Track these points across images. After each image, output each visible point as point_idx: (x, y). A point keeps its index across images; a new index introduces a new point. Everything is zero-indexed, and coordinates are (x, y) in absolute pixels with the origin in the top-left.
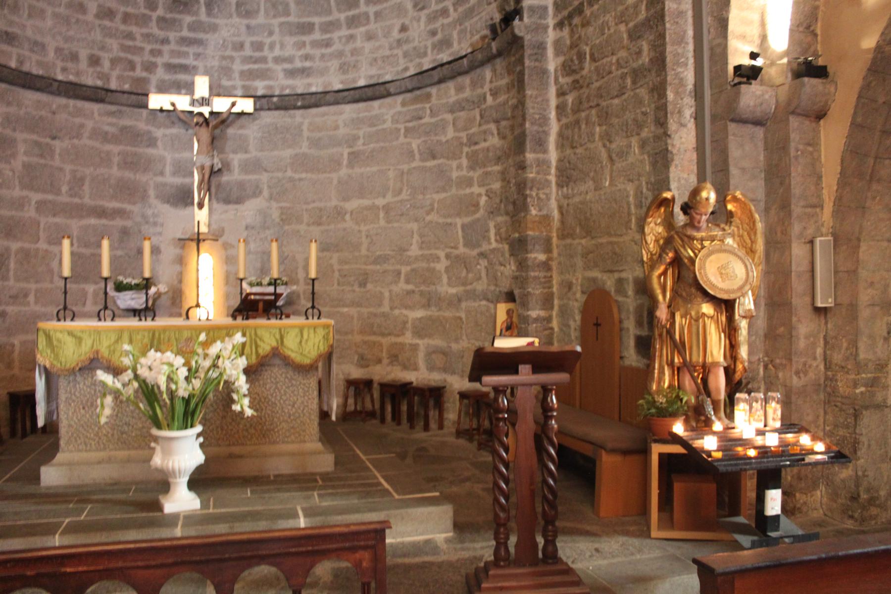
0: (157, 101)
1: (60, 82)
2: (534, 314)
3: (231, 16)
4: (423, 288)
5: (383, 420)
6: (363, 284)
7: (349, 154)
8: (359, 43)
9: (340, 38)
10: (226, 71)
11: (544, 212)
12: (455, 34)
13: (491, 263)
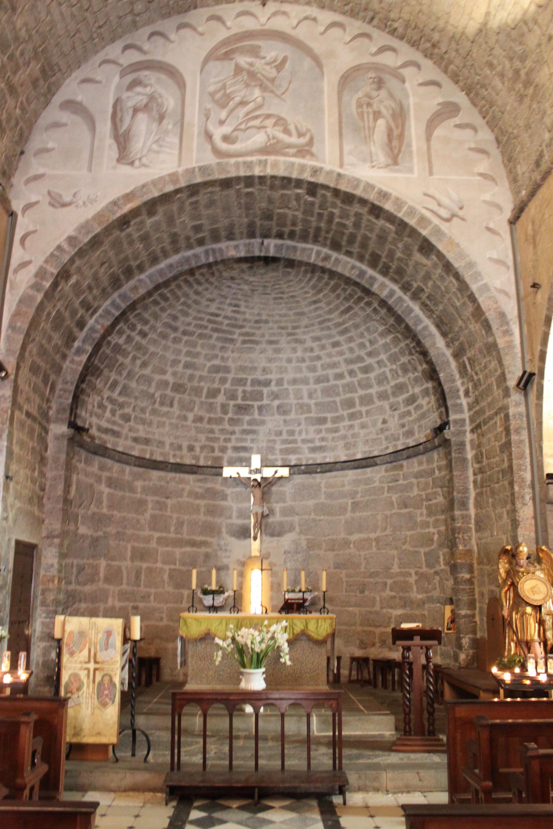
0: (228, 472)
1: (172, 464)
2: (463, 612)
3: (274, 414)
4: (401, 594)
5: (375, 686)
6: (362, 592)
7: (352, 503)
8: (356, 430)
9: (344, 427)
10: (271, 450)
11: (468, 548)
12: (416, 427)
13: (441, 578)
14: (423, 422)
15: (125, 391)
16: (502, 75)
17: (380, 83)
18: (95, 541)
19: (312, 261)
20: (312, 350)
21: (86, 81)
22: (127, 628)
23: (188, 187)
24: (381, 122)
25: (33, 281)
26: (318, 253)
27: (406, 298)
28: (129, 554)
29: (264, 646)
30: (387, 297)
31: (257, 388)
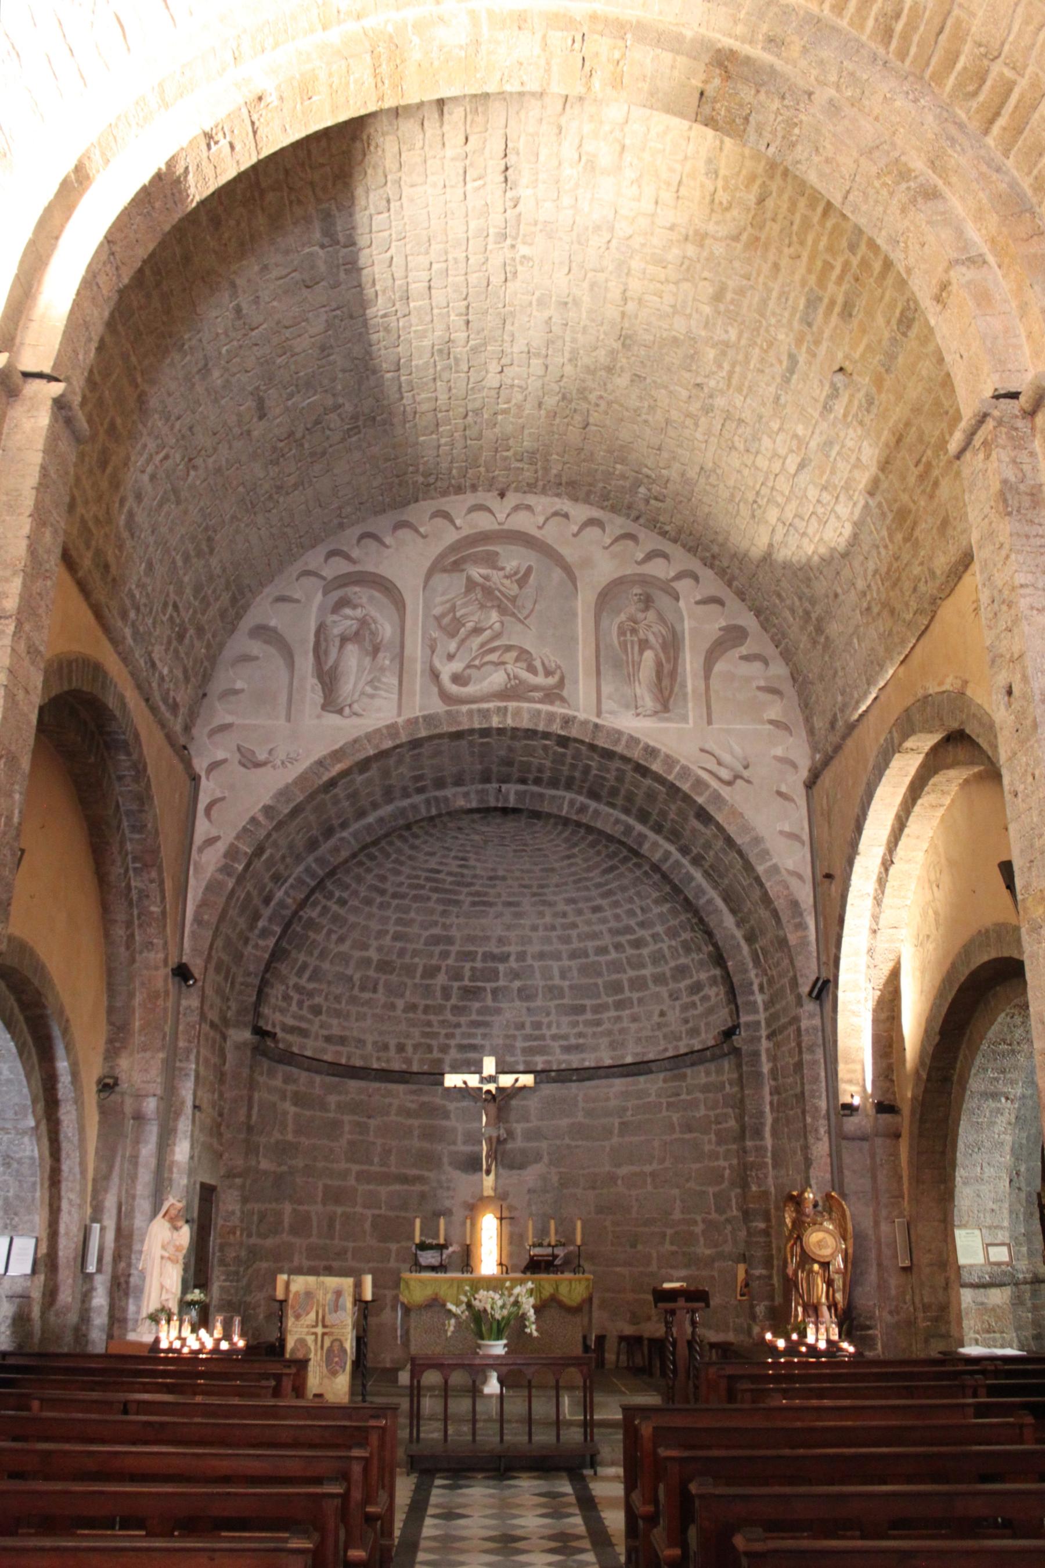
0: (452, 1080)
2: (757, 1272)
6: (634, 1246)
8: (625, 1024)
9: (609, 1018)
10: (510, 1049)
14: (711, 1018)
15: (316, 975)
16: (793, 611)
17: (647, 602)
18: (279, 1179)
19: (564, 813)
20: (564, 915)
21: (282, 599)
22: (358, 1286)
23: (410, 742)
24: (649, 655)
25: (223, 861)
26: (572, 803)
27: (685, 862)
28: (320, 1194)
29: (505, 1312)
30: (660, 860)
31: (490, 964)
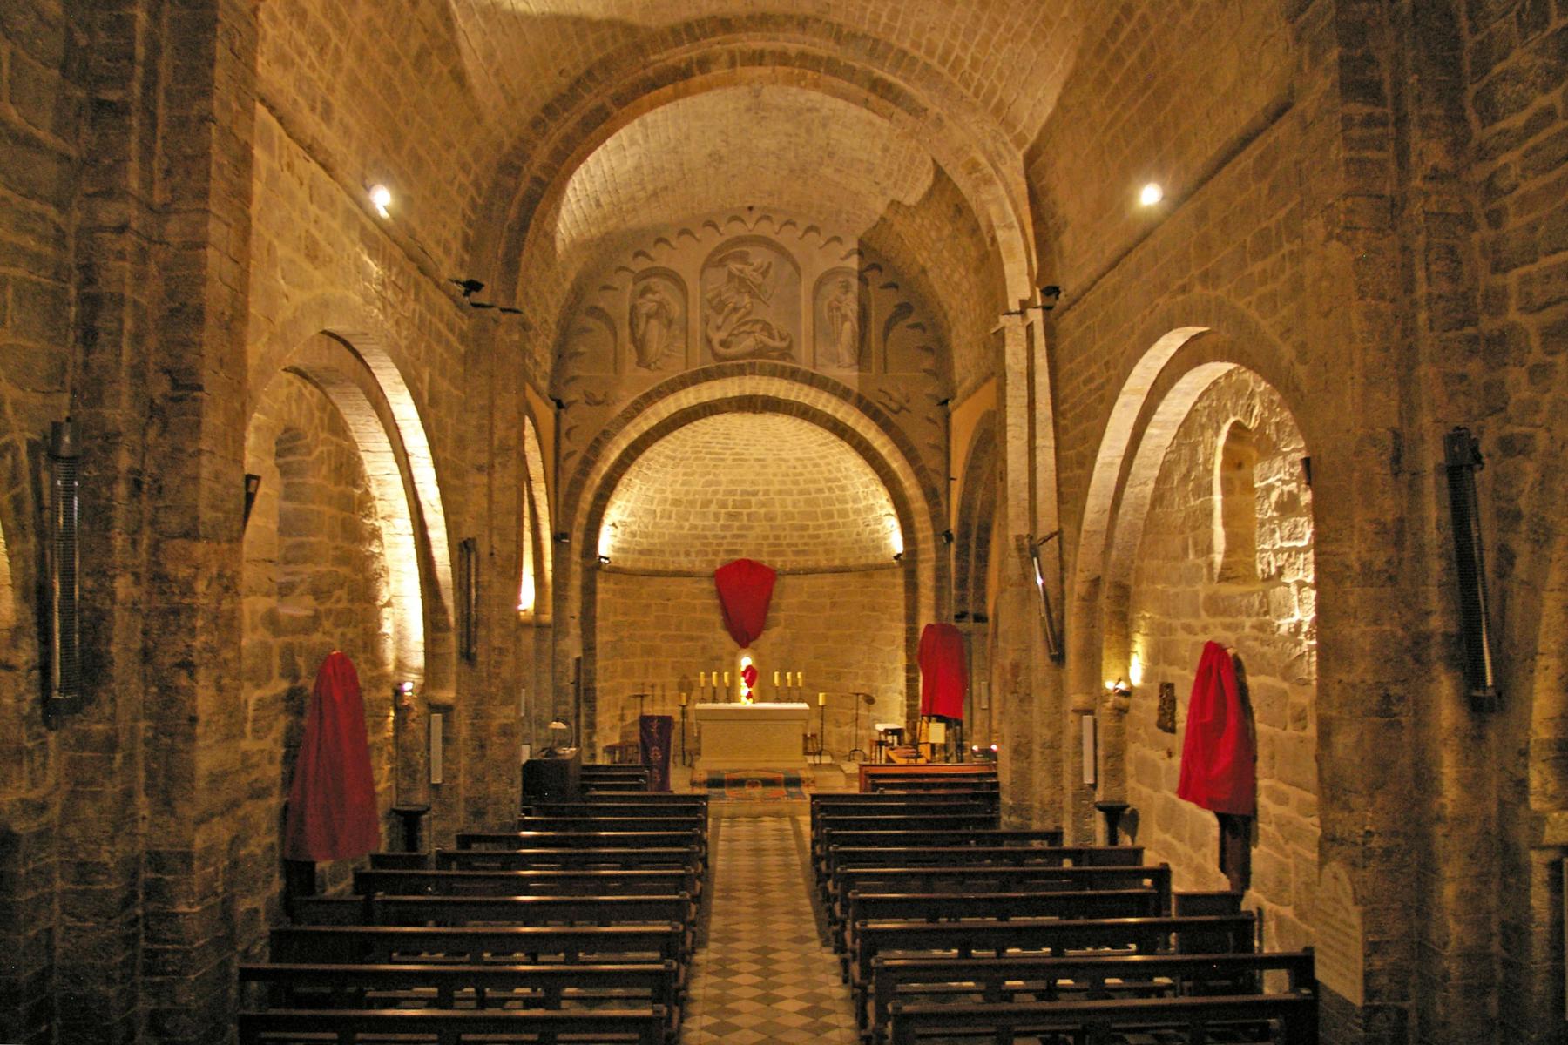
21: (606, 288)
24: (847, 325)
